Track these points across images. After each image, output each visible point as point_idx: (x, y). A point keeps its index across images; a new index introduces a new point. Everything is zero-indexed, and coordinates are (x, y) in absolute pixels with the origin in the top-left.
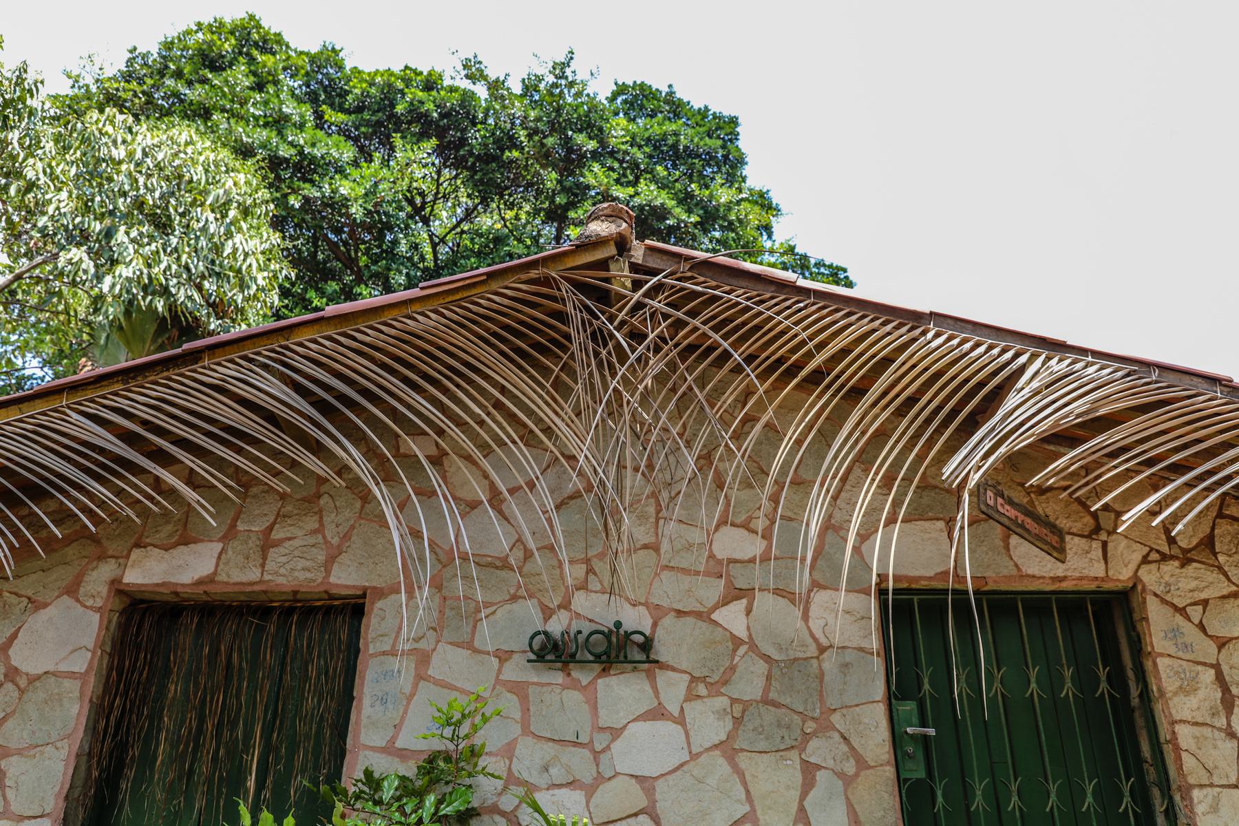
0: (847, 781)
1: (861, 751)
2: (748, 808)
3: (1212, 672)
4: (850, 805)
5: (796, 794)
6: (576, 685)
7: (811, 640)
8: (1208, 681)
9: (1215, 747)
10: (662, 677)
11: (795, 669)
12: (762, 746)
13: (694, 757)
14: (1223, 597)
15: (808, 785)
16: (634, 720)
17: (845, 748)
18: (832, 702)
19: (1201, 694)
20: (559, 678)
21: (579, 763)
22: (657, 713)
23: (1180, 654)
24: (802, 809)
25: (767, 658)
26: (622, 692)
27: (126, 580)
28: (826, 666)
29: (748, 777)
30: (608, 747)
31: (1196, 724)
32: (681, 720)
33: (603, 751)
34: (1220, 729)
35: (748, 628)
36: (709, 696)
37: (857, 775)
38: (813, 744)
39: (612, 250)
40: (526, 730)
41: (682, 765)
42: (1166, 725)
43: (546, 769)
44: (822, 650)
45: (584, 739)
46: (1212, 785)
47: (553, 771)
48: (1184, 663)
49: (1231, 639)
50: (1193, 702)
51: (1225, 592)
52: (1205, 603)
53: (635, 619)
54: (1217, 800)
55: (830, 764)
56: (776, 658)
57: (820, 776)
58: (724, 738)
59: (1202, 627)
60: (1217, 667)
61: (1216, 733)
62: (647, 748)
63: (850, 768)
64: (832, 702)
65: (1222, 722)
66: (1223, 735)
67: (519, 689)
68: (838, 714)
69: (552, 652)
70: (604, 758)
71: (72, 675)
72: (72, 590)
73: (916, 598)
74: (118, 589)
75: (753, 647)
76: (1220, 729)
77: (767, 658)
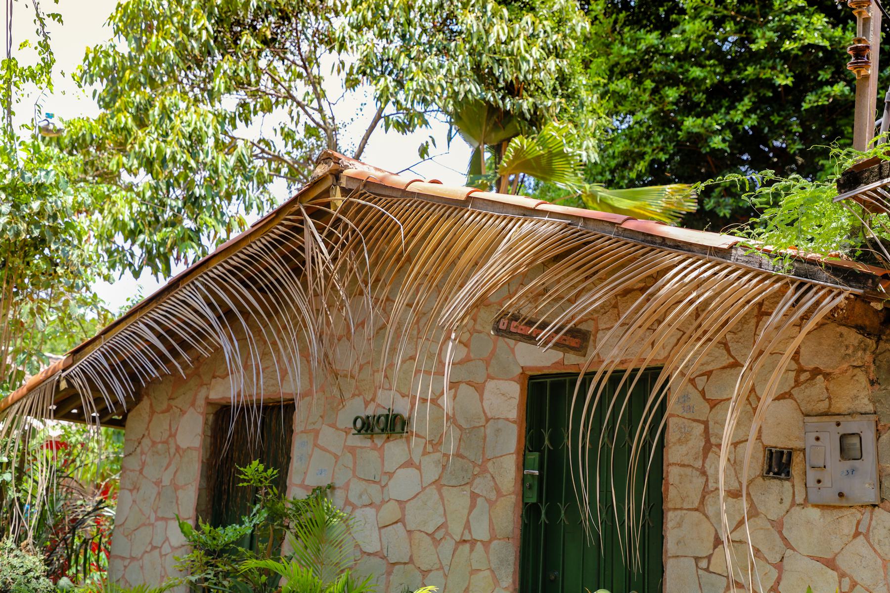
0: (491, 503)
1: (500, 485)
2: (444, 520)
3: (703, 426)
4: (490, 519)
5: (466, 511)
6: (375, 448)
7: (482, 414)
8: (698, 434)
9: (691, 482)
11: (473, 432)
12: (453, 483)
13: (424, 489)
14: (724, 368)
15: (473, 506)
16: (400, 467)
17: (492, 484)
18: (488, 455)
19: (690, 444)
20: (368, 443)
21: (374, 491)
22: (409, 464)
23: (685, 414)
24: (468, 521)
25: (460, 427)
26: (395, 450)
27: (210, 397)
28: (488, 431)
29: (446, 502)
30: (387, 484)
31: (684, 466)
32: (419, 468)
33: (385, 486)
34: (697, 469)
35: (454, 409)
36: (434, 452)
37: (496, 501)
38: (477, 481)
39: (330, 181)
41: (418, 494)
43: (360, 496)
44: (487, 420)
45: (377, 479)
46: (681, 509)
47: (364, 497)
48: (686, 421)
49: (722, 401)
50: (683, 449)
51: (724, 364)
52: (709, 374)
53: (402, 407)
54: (682, 519)
55: (485, 494)
57: (480, 501)
58: (437, 478)
59: (703, 393)
60: (706, 423)
61: (694, 471)
62: (404, 484)
63: (493, 496)
64: (488, 455)
65: (699, 464)
66: (698, 473)
67: (352, 450)
68: (491, 462)
69: (366, 427)
70: (386, 489)
71: (195, 449)
72: (193, 404)
73: (548, 380)
74: (209, 403)
76: (697, 469)
77: (460, 427)
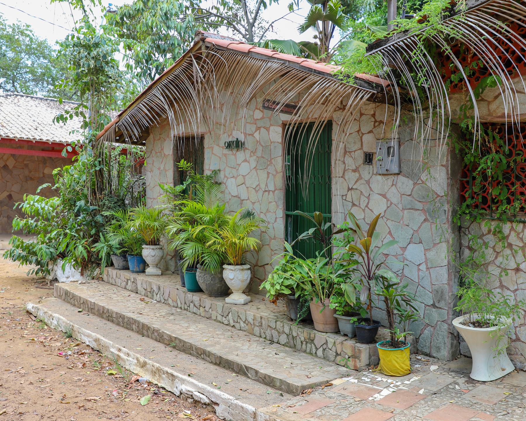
0: (274, 176)
10: (247, 151)
12: (261, 168)
22: (245, 161)
32: (249, 162)
40: (227, 166)
42: (237, 358)
56: (331, 46)
57: (270, 175)
63: (275, 173)
64: (273, 157)
67: (225, 155)
69: (229, 145)
75: (260, 143)
